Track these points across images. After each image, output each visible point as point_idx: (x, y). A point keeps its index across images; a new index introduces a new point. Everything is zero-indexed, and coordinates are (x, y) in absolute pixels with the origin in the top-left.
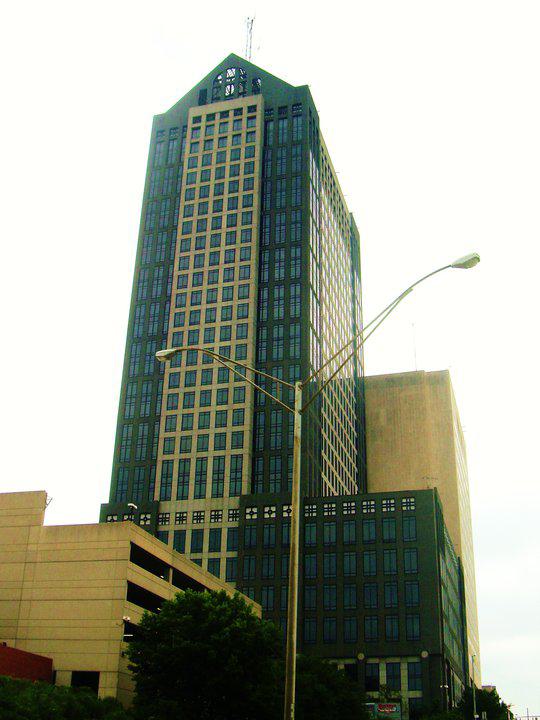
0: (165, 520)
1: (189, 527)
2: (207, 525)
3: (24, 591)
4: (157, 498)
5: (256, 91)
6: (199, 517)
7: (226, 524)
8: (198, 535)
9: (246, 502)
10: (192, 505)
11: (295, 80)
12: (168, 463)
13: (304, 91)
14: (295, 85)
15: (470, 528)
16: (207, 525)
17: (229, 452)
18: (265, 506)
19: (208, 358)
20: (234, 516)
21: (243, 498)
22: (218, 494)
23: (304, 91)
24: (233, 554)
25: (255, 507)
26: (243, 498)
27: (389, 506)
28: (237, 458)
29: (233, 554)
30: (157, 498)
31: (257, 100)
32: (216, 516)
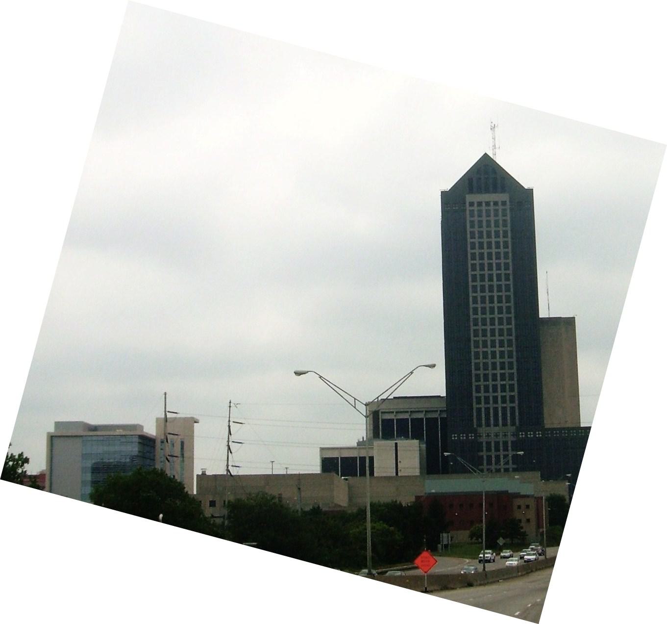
0: (480, 436)
1: (492, 439)
2: (501, 439)
3: (288, 470)
4: (475, 426)
5: (503, 190)
6: (497, 435)
7: (510, 439)
8: (497, 444)
9: (519, 429)
10: (493, 430)
11: (525, 183)
12: (479, 410)
13: (530, 192)
14: (526, 188)
15: (47, 464)
16: (501, 439)
17: (508, 405)
18: (461, 433)
19: (485, 355)
20: (513, 435)
21: (517, 427)
22: (505, 424)
23: (530, 192)
24: (481, 454)
25: (532, 431)
26: (517, 427)
27: (565, 433)
28: (513, 409)
29: (481, 454)
30: (475, 426)
31: (505, 197)
32: (497, 435)
